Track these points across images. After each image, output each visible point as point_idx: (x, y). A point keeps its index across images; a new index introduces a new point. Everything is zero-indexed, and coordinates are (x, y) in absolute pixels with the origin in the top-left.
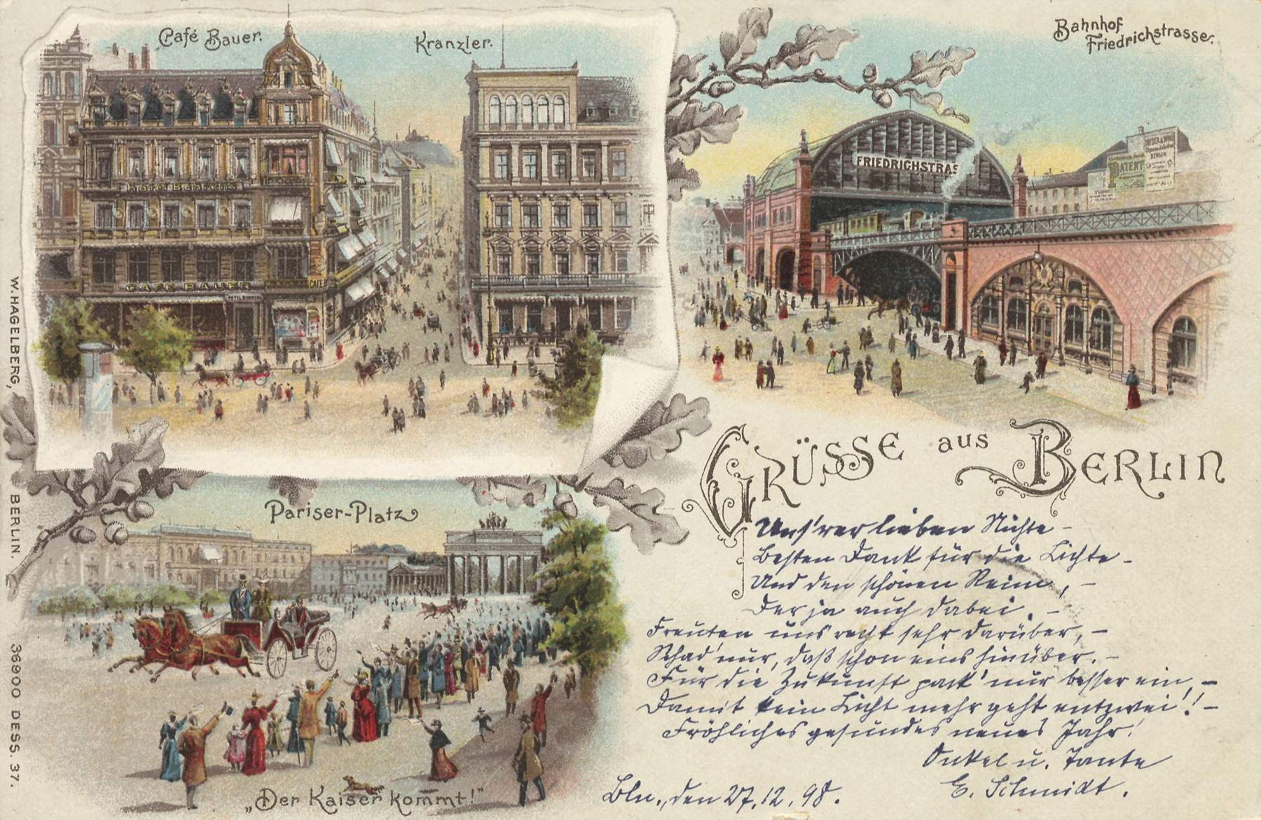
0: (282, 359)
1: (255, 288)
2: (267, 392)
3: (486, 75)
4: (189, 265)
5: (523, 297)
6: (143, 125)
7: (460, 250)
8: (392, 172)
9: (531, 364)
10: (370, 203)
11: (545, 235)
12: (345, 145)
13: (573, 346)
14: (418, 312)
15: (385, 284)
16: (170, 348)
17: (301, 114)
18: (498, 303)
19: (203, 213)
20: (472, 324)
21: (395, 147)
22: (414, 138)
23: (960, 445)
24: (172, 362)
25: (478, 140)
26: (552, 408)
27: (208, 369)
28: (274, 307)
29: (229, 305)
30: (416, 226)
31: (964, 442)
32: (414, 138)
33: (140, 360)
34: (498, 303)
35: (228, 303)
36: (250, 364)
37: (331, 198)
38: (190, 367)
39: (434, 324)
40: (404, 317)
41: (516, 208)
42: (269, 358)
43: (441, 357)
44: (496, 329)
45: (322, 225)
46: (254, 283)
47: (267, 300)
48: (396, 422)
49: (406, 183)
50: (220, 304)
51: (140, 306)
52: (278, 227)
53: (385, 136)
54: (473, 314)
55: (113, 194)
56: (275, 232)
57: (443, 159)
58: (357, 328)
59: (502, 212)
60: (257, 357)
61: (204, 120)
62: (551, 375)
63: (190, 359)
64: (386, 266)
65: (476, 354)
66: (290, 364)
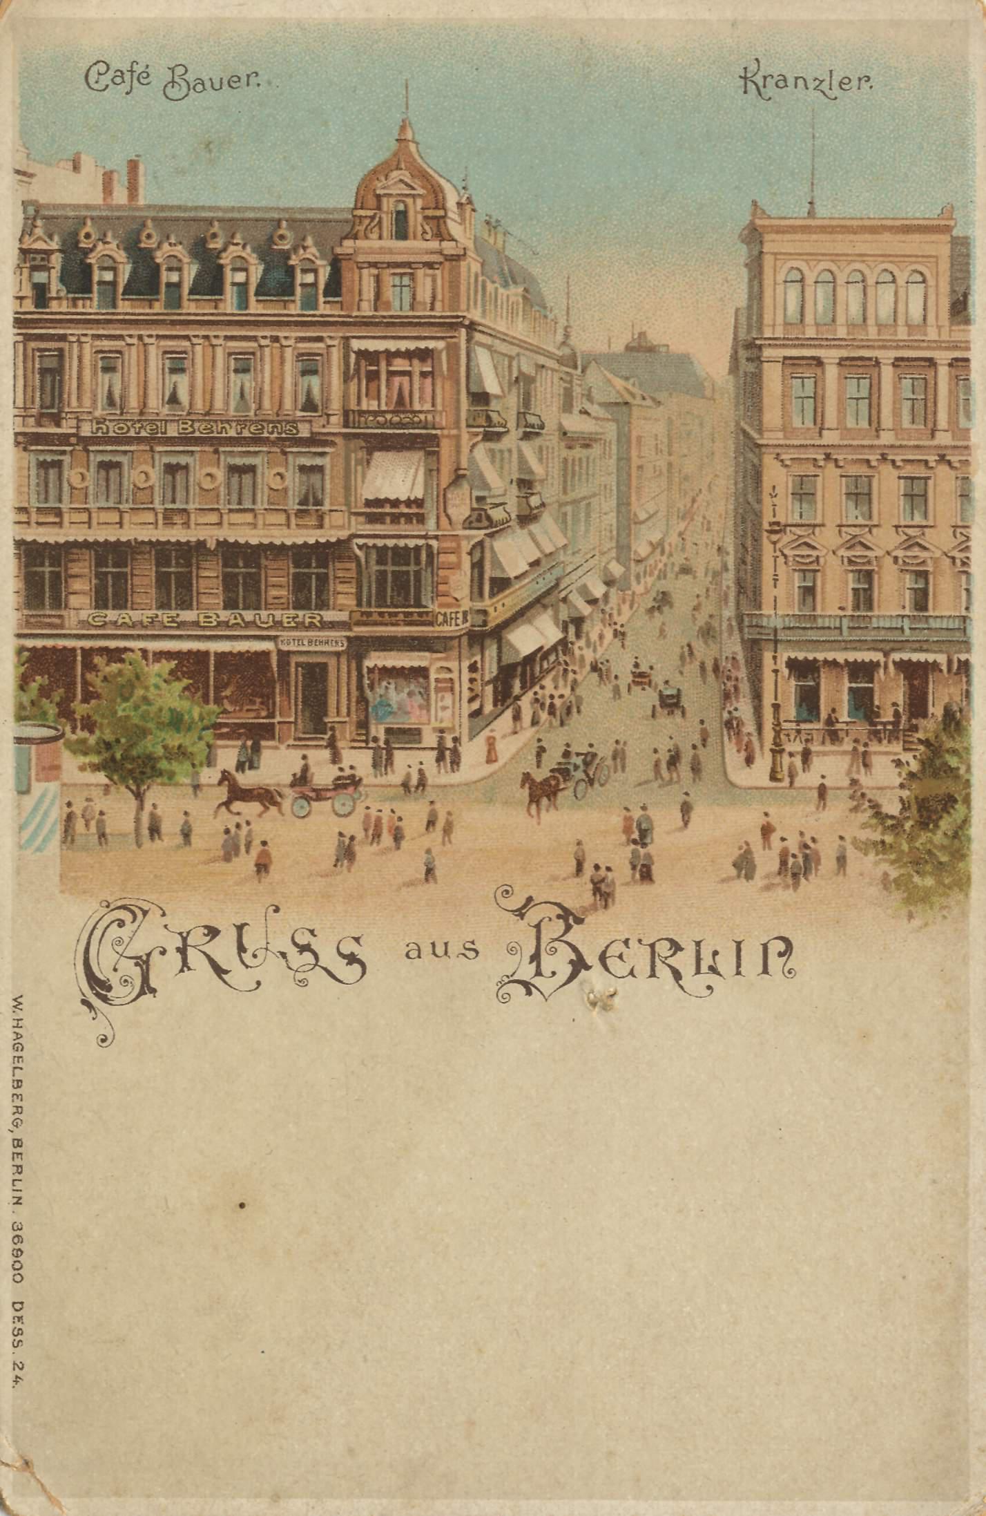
0: (382, 761)
1: (333, 625)
2: (353, 826)
3: (780, 230)
4: (209, 576)
5: (840, 657)
6: (124, 307)
7: (725, 568)
8: (594, 409)
9: (854, 782)
10: (556, 471)
11: (885, 540)
12: (511, 358)
13: (934, 748)
14: (641, 678)
15: (578, 621)
16: (174, 740)
17: (424, 294)
18: (792, 664)
19: (235, 479)
20: (744, 709)
21: (607, 360)
22: (641, 348)
23: (434, 953)
24: (175, 766)
25: (760, 347)
26: (894, 874)
27: (246, 779)
28: (368, 663)
29: (284, 656)
30: (642, 516)
31: (440, 950)
32: (641, 348)
33: (113, 759)
34: (792, 664)
35: (279, 652)
36: (324, 774)
37: (481, 453)
38: (209, 776)
39: (671, 703)
40: (616, 691)
41: (831, 485)
42: (359, 760)
43: (684, 767)
44: (790, 710)
45: (460, 507)
46: (329, 615)
47: (358, 648)
48: (596, 890)
49: (624, 439)
50: (266, 654)
51: (115, 655)
52: (377, 510)
53: (587, 341)
54: (745, 687)
55: (64, 439)
56: (373, 519)
57: (698, 388)
58: (526, 703)
59: (803, 493)
60: (336, 758)
61: (243, 303)
62: (892, 808)
63: (210, 762)
64: (584, 591)
65: (749, 760)
66: (396, 778)
